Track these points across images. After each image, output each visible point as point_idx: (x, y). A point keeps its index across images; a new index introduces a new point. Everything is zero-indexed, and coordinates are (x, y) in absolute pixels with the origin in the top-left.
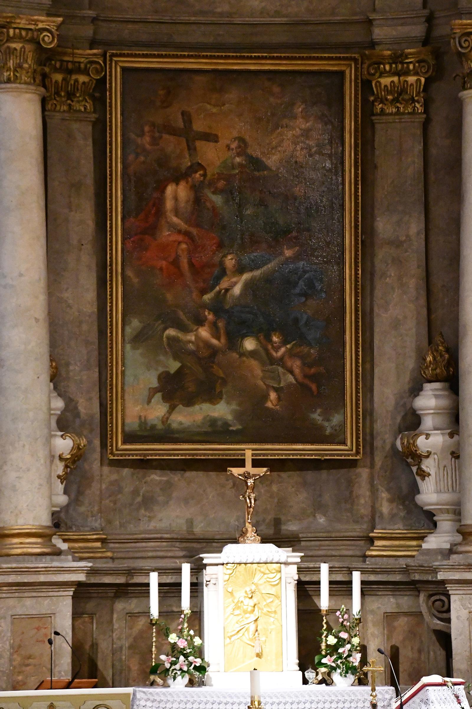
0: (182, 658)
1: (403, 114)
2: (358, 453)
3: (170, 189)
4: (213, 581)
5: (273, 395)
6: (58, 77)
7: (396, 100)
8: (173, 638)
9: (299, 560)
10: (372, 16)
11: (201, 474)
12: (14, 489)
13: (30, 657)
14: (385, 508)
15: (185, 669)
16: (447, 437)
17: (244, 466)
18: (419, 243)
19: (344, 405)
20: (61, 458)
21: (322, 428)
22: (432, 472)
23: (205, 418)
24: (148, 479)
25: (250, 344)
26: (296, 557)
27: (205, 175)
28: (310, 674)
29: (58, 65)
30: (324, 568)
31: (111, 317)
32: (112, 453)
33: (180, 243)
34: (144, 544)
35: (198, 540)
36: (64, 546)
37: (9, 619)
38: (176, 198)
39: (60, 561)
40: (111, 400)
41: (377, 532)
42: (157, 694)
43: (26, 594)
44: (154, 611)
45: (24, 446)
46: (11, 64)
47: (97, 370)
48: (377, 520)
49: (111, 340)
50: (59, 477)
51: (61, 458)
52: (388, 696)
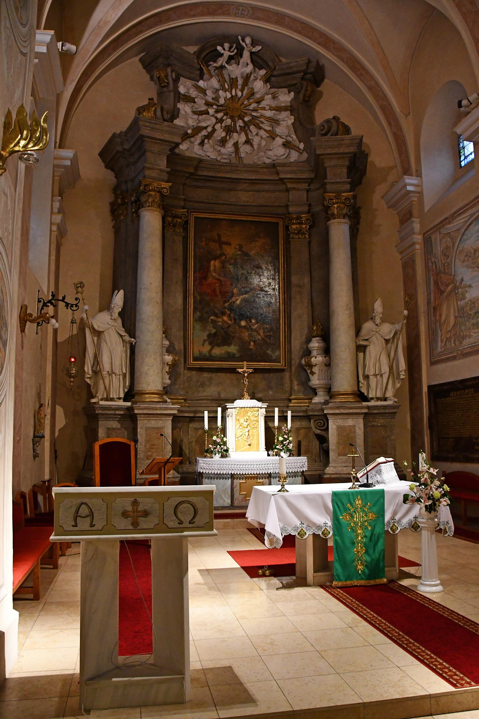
0: (218, 446)
1: (301, 238)
2: (285, 366)
3: (212, 263)
4: (231, 415)
5: (252, 343)
6: (170, 219)
7: (298, 234)
8: (215, 438)
9: (266, 406)
10: (289, 204)
11: (223, 374)
12: (147, 374)
13: (154, 445)
14: (296, 388)
15: (220, 451)
16: (324, 358)
17: (243, 368)
18: (308, 286)
19: (280, 348)
20: (167, 364)
21: (271, 356)
22: (317, 372)
23: (225, 352)
24: (203, 376)
25: (243, 323)
26: (265, 405)
27: (226, 258)
28: (271, 452)
29: (170, 215)
30: (276, 410)
31: (189, 311)
32: (188, 365)
33: (216, 283)
34: (201, 401)
35: (223, 400)
36: (169, 400)
37: (144, 429)
38: (215, 266)
39: (167, 405)
40: (188, 344)
41: (293, 397)
42: (208, 461)
43: (152, 419)
44: (206, 427)
45: (151, 356)
46: (150, 200)
47: (183, 332)
48: (293, 392)
49: (189, 320)
50: (167, 372)
51: (167, 364)
52: (304, 461)
